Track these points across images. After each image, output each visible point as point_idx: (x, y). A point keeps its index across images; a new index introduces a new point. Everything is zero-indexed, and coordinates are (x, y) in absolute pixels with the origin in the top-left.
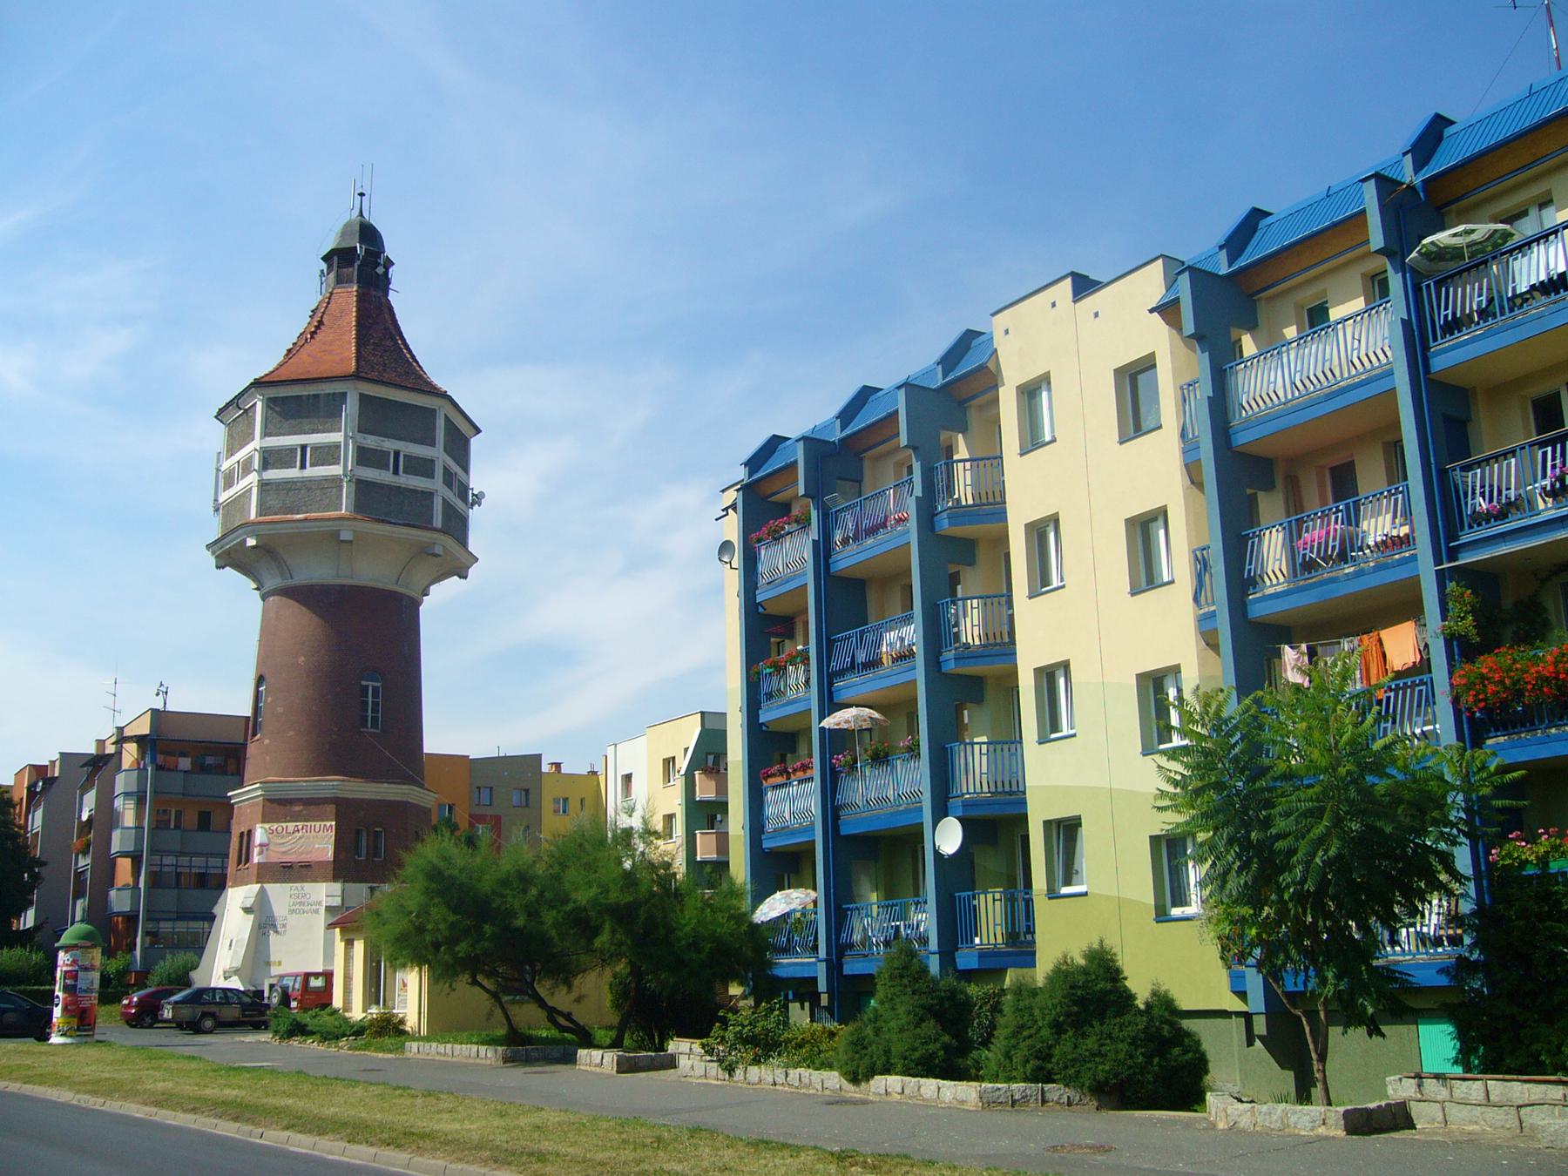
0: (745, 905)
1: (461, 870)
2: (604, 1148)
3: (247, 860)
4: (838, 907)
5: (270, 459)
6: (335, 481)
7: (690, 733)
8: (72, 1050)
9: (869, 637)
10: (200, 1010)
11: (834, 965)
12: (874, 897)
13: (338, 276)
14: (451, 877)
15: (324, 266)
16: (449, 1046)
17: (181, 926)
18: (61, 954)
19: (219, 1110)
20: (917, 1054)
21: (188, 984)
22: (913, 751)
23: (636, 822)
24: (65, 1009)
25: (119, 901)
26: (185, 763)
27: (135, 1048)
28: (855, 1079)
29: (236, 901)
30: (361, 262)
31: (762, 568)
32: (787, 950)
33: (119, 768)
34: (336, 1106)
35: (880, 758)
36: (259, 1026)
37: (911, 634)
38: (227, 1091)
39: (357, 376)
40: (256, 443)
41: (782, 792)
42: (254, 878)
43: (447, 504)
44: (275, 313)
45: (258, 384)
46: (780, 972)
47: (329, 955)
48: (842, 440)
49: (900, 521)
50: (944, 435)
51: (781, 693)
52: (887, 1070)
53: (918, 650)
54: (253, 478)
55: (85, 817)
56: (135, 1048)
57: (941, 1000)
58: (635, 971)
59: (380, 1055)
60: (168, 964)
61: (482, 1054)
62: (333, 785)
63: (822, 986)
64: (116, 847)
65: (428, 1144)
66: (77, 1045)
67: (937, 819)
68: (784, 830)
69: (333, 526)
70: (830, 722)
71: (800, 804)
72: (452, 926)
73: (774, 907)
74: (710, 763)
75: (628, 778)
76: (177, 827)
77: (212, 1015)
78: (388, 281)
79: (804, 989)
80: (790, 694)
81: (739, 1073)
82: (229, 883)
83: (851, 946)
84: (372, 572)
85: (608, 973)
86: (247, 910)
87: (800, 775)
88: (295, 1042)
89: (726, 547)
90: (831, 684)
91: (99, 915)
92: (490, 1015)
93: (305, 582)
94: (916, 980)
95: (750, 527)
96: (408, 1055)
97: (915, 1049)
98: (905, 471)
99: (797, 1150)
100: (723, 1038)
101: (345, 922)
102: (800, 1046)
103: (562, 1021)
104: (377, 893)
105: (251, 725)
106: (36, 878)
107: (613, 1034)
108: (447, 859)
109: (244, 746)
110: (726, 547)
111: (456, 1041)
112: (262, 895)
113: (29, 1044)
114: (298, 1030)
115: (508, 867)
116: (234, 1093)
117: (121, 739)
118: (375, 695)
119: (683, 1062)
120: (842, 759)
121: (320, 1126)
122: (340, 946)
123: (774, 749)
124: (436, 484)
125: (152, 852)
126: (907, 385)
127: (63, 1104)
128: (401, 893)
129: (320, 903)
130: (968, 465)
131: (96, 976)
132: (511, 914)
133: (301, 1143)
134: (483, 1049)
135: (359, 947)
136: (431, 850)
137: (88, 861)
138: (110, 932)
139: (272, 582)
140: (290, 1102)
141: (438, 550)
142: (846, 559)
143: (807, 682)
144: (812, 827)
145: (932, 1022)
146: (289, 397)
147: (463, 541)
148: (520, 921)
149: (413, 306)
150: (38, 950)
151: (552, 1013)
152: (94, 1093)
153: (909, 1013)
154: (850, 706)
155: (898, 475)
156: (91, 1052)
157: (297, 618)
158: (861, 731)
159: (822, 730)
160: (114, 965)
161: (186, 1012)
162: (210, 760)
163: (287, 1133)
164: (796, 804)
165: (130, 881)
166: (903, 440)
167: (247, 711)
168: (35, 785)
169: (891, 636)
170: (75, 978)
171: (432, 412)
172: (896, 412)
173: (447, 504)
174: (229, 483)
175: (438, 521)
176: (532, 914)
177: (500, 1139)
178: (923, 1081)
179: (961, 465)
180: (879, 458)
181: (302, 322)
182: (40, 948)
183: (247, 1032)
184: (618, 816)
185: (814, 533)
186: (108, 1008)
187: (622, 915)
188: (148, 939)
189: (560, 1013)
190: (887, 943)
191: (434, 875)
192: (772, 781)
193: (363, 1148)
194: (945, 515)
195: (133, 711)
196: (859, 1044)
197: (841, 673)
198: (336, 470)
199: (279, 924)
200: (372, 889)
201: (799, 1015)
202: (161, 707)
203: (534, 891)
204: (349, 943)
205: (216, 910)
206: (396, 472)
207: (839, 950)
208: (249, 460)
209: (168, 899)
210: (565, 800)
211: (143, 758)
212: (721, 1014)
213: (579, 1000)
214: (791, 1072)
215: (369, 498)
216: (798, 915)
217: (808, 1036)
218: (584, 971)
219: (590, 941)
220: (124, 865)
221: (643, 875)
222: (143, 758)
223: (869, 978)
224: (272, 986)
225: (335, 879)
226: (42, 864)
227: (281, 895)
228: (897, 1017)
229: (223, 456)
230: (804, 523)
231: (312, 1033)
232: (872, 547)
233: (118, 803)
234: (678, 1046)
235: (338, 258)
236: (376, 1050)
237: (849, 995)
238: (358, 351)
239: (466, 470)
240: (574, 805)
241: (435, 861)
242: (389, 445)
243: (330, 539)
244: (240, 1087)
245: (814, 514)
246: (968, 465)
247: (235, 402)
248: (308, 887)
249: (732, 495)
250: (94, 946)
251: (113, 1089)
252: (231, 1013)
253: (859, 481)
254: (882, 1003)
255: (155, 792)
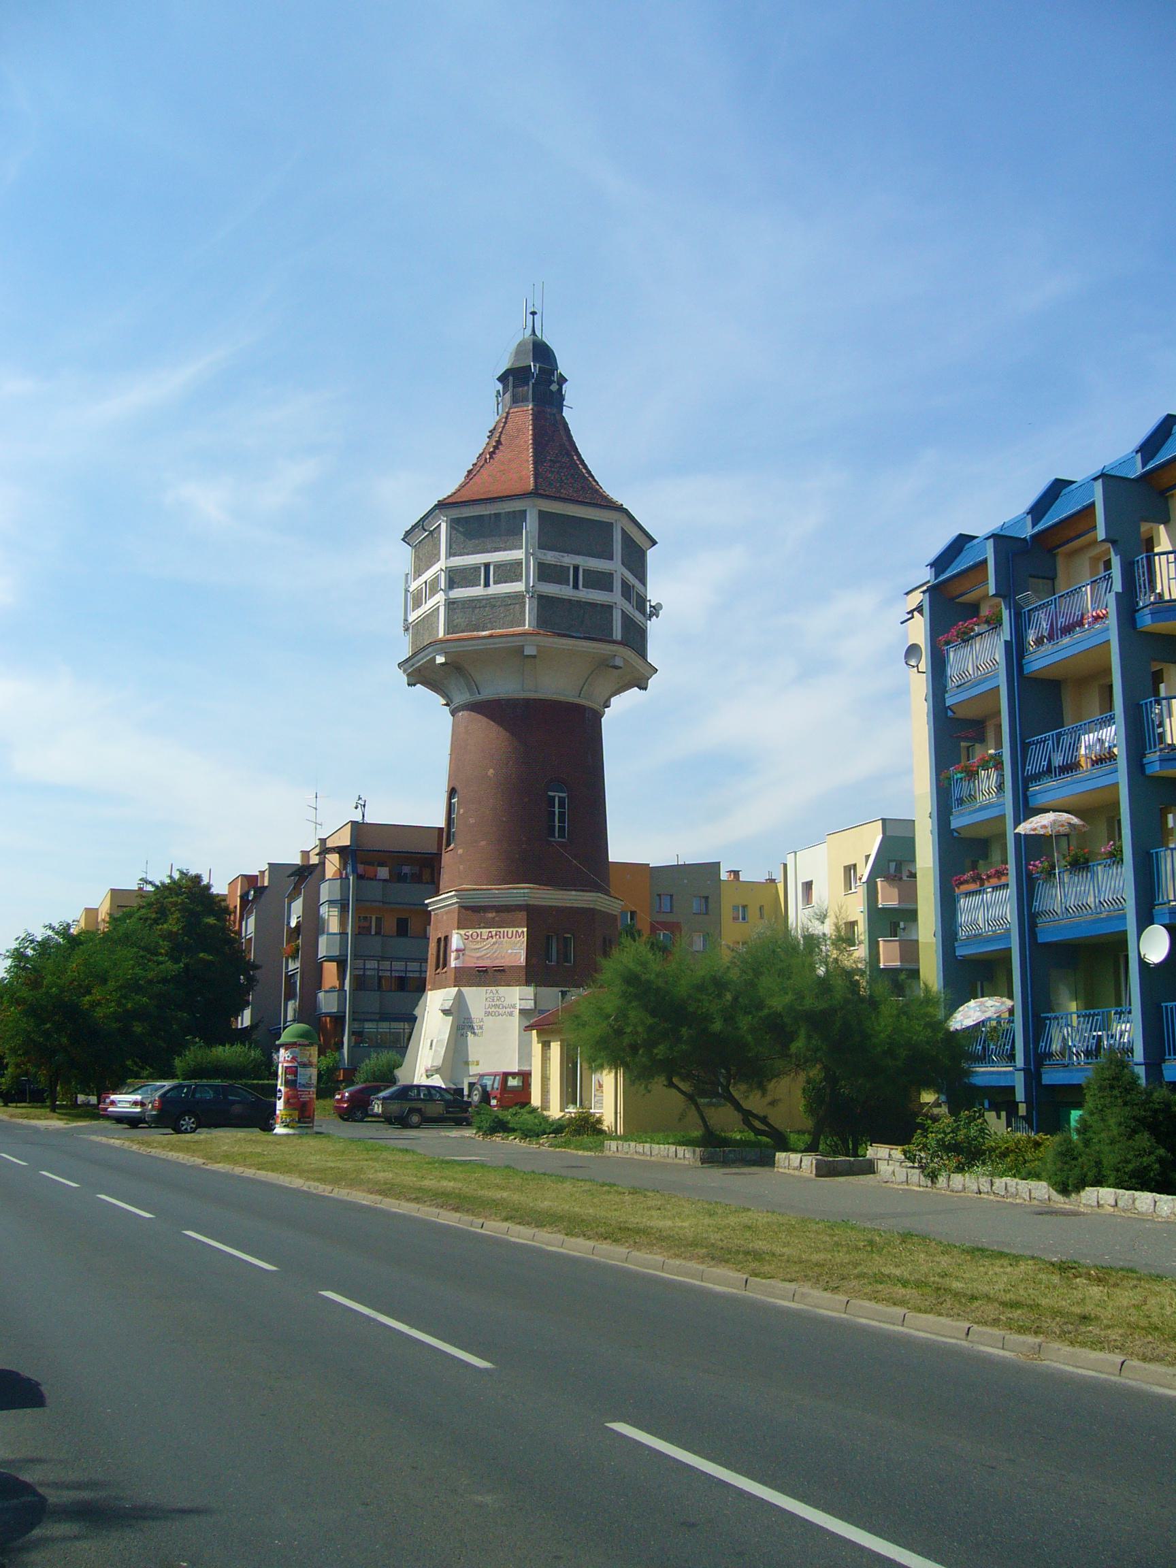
0: (941, 1014)
1: (658, 975)
2: (818, 1250)
3: (445, 965)
4: (1036, 1016)
5: (456, 578)
6: (518, 598)
7: (873, 840)
8: (296, 1140)
9: (1067, 740)
10: (407, 1106)
11: (1032, 1075)
12: (1073, 1006)
13: (514, 396)
14: (648, 981)
15: (500, 387)
16: (647, 1145)
17: (384, 1026)
18: (282, 1051)
19: (439, 1201)
20: (1131, 1167)
21: (393, 1081)
22: (1115, 857)
23: (828, 928)
24: (287, 1103)
25: (327, 1002)
26: (383, 872)
27: (352, 1140)
28: (1064, 1190)
29: (435, 1004)
30: (535, 381)
31: (952, 671)
32: (983, 1058)
33: (322, 878)
34: (549, 1199)
35: (1080, 865)
36: (461, 1122)
37: (1112, 735)
38: (445, 1183)
39: (536, 493)
40: (441, 564)
41: (976, 899)
42: (452, 981)
43: (626, 617)
44: (453, 437)
45: (442, 505)
46: (978, 1081)
47: (525, 1054)
48: (1033, 537)
49: (1097, 618)
50: (1144, 527)
51: (972, 797)
52: (1098, 1182)
53: (1120, 751)
54: (440, 598)
55: (293, 924)
56: (352, 1140)
57: (1155, 1111)
58: (832, 1079)
59: (580, 1153)
60: (374, 1061)
61: (680, 1154)
62: (523, 892)
63: (1020, 1095)
64: (322, 952)
65: (644, 1240)
66: (300, 1135)
67: (1142, 927)
68: (976, 938)
69: (518, 642)
70: (1024, 828)
71: (995, 912)
72: (651, 1029)
73: (969, 1015)
74: (892, 870)
75: (808, 886)
76: (378, 933)
77: (419, 1111)
78: (562, 398)
79: (1001, 1099)
80: (981, 799)
81: (942, 1180)
82: (428, 987)
83: (1050, 1055)
84: (555, 685)
85: (802, 1077)
86: (446, 1012)
87: (994, 881)
88: (497, 1138)
89: (912, 650)
90: (1026, 788)
91: (308, 1012)
92: (682, 1117)
93: (491, 697)
94: (1127, 1091)
95: (937, 630)
96: (607, 1153)
97: (1128, 1162)
98: (1102, 567)
99: (1016, 1259)
100: (925, 1146)
101: (541, 1024)
102: (1004, 1155)
103: (757, 1124)
104: (568, 997)
105: (444, 836)
106: (251, 980)
107: (807, 1138)
108: (644, 964)
109: (438, 856)
110: (912, 650)
111: (653, 1141)
112: (460, 998)
113: (256, 1134)
114: (500, 1127)
115: (701, 973)
116: (452, 1184)
117: (324, 850)
118: (562, 805)
119: (882, 1167)
120: (1040, 865)
121: (539, 1219)
122: (537, 1048)
123: (966, 856)
124: (615, 597)
125: (356, 956)
126: (1103, 476)
127: (294, 1189)
128: (595, 999)
129: (514, 1006)
130: (1171, 557)
131: (314, 1072)
132: (708, 1018)
133: (520, 1234)
134: (681, 1149)
135: (555, 1048)
136: (628, 956)
137: (298, 965)
138: (324, 1032)
139: (461, 698)
140: (505, 1194)
141: (618, 662)
142: (1040, 659)
143: (1000, 787)
144: (1007, 935)
145: (1146, 1135)
146: (471, 517)
147: (642, 653)
148: (717, 1026)
149: (579, 416)
150: (257, 1046)
151: (747, 1117)
152: (322, 1180)
153: (1120, 1124)
154: (1047, 811)
155: (1094, 571)
156: (312, 1143)
157: (485, 731)
158: (1059, 836)
159: (1017, 836)
160: (326, 1062)
161: (394, 1107)
162: (406, 869)
163: (506, 1225)
164: (991, 911)
165: (336, 983)
166: (1101, 534)
167: (441, 823)
168: (247, 893)
169: (1089, 738)
170: (295, 1073)
171: (610, 526)
172: (1093, 504)
173: (626, 617)
174: (417, 603)
175: (618, 634)
176: (729, 1019)
177: (714, 1237)
178: (1137, 1194)
179: (1164, 557)
180: (1072, 554)
181: (480, 443)
182: (257, 1045)
183: (450, 1128)
184: (799, 918)
185: (1006, 633)
186: (322, 1102)
187: (818, 1021)
188: (353, 1038)
189: (756, 1117)
190: (1088, 1053)
191: (631, 979)
192: (964, 888)
193: (581, 1241)
194: (1147, 611)
195: (335, 823)
196: (1068, 1154)
197: (1037, 777)
198: (519, 587)
199: (476, 1024)
200: (564, 993)
201: (996, 1124)
202: (359, 819)
203: (729, 997)
204: (546, 1045)
205: (417, 1012)
206: (576, 586)
207: (1038, 1059)
208: (436, 580)
209: (372, 1001)
210: (744, 907)
211: (345, 868)
212: (919, 1120)
213: (773, 1103)
214: (997, 1181)
215: (552, 613)
216: (994, 1023)
217: (1011, 1145)
218: (777, 1076)
219: (786, 1046)
220: (330, 969)
221: (839, 983)
222: (345, 868)
223: (1078, 1088)
224: (471, 1085)
225: (528, 983)
226: (256, 967)
227: (477, 997)
228: (1108, 1128)
229: (411, 577)
230: (994, 623)
231: (514, 1130)
232: (1068, 646)
233: (324, 910)
234: (877, 1152)
235: (513, 378)
236: (577, 1148)
237: (1049, 1106)
238: (535, 468)
239: (643, 580)
240: (753, 912)
241: (631, 966)
242: (569, 560)
243: (514, 655)
244: (455, 1179)
245: (1005, 614)
246: (1171, 557)
247: (421, 524)
248: (502, 990)
249: (917, 598)
250: (311, 1044)
251: (338, 1178)
252: (435, 1109)
253: (1053, 579)
254: (1091, 1114)
255: (357, 900)
